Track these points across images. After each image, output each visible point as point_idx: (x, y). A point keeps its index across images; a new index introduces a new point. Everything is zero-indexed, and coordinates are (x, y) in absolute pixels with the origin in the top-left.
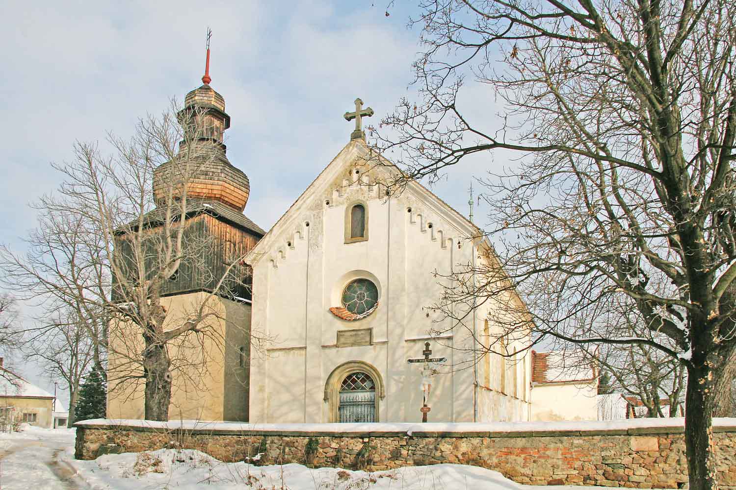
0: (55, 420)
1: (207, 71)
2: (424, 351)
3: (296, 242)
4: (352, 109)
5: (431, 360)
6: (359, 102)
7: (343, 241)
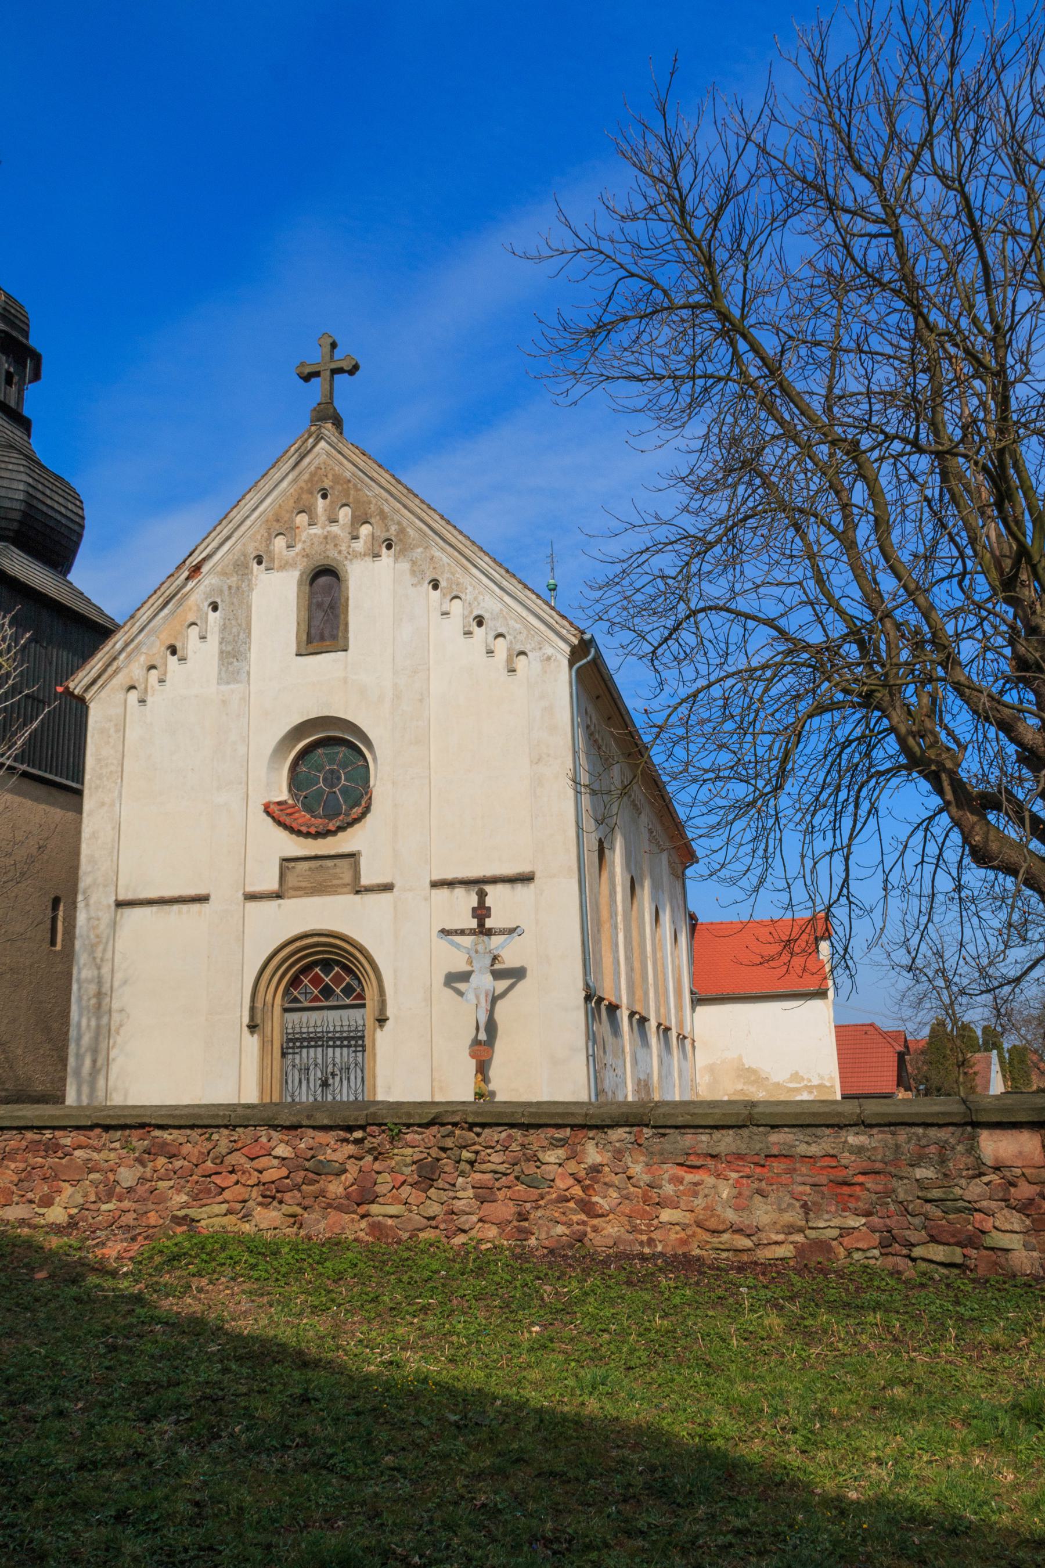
4: (316, 357)
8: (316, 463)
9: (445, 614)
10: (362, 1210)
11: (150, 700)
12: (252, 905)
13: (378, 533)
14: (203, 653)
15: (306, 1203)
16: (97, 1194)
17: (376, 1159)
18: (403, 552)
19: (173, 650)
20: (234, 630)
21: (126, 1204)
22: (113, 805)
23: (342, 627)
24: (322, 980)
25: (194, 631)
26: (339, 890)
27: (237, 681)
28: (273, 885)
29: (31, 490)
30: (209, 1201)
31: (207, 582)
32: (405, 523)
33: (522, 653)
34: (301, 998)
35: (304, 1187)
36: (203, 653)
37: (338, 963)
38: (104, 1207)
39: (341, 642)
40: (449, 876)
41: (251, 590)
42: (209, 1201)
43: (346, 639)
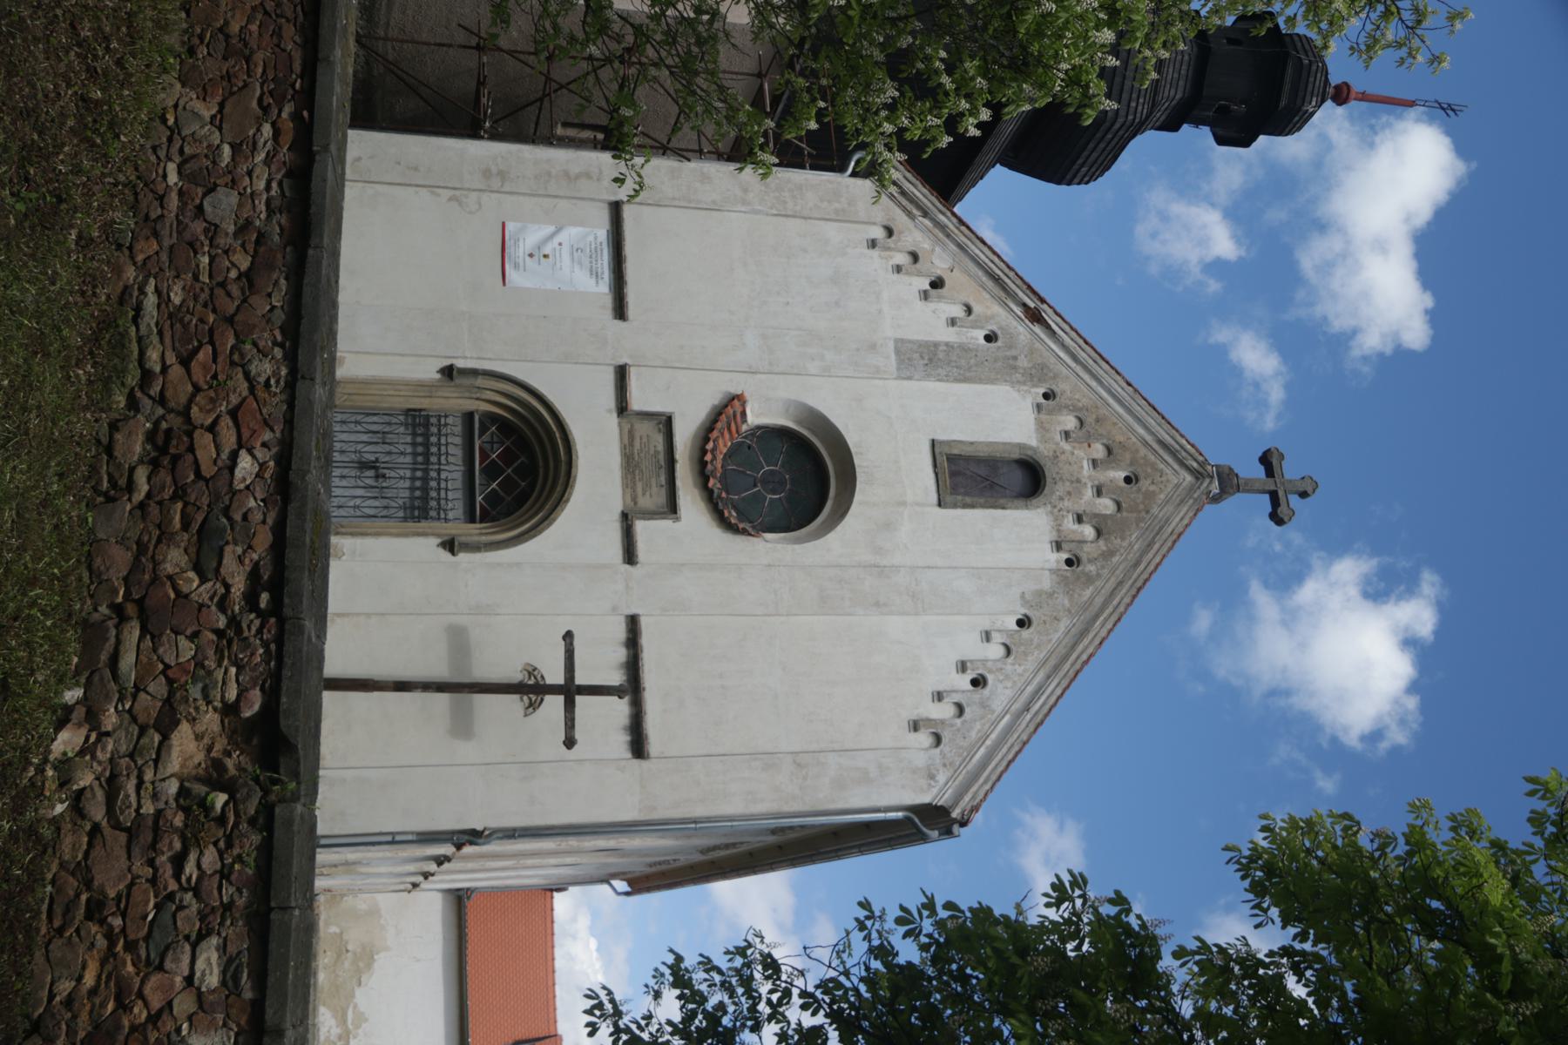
4: (1291, 470)
7: (941, 437)
8: (1168, 471)
9: (987, 637)
10: (131, 609)
11: (875, 253)
12: (609, 378)
13: (1087, 548)
14: (931, 322)
15: (154, 510)
16: (194, 156)
17: (220, 633)
18: (1064, 581)
19: (937, 284)
20: (963, 362)
21: (173, 201)
22: (744, 202)
23: (968, 500)
24: (511, 466)
25: (958, 311)
26: (629, 491)
27: (900, 362)
28: (637, 402)
29: (1107, 124)
30: (168, 340)
31: (1021, 329)
32: (1099, 583)
33: (938, 740)
34: (486, 437)
35: (180, 505)
36: (931, 322)
37: (532, 486)
38: (172, 168)
39: (949, 499)
40: (645, 641)
41: (1013, 384)
42: (168, 340)
43: (955, 506)
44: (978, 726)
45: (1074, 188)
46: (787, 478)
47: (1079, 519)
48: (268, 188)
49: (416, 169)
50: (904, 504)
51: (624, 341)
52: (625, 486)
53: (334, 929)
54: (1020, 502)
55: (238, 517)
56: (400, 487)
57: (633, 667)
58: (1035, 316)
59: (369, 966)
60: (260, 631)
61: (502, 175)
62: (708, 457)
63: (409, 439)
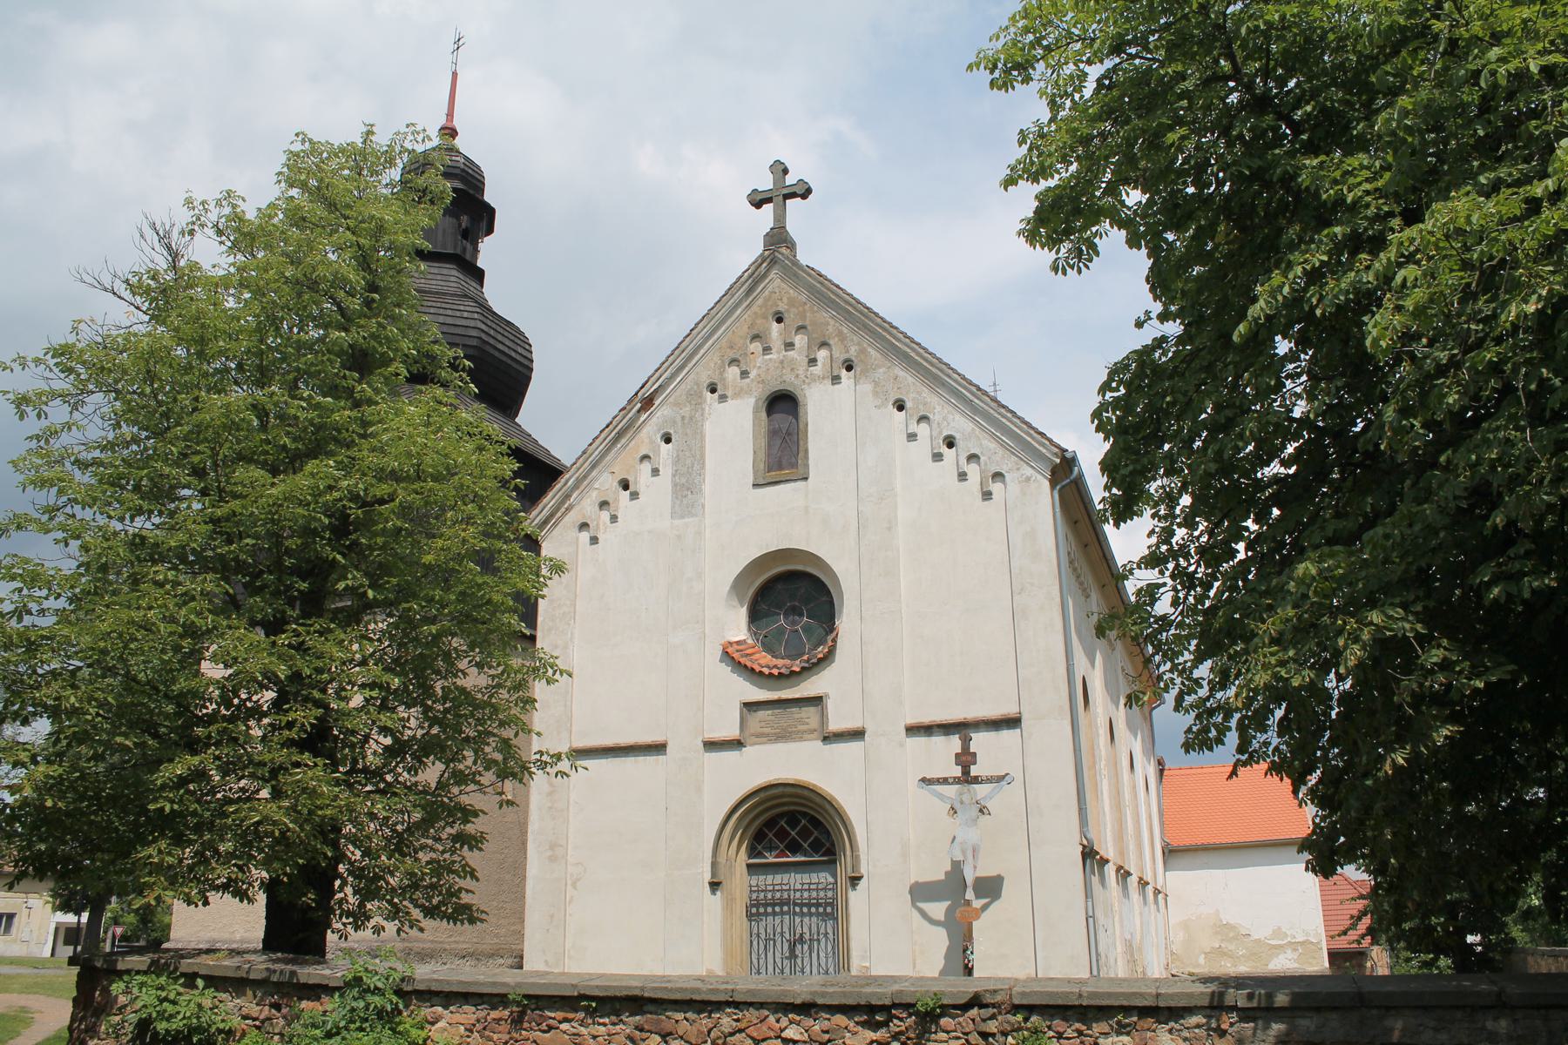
0: (57, 929)
1: (450, 115)
2: (992, 84)
3: (642, 478)
4: (766, 183)
5: (976, 780)
6: (780, 169)
7: (751, 480)
9: (912, 437)
20: (688, 462)
25: (646, 467)
29: (484, 336)
36: (655, 490)
37: (805, 814)
39: (801, 470)
43: (807, 466)
44: (985, 442)
45: (534, 357)
46: (792, 600)
47: (813, 361)
48: (604, 1025)
49: (552, 916)
50: (806, 508)
51: (684, 744)
52: (801, 739)
53: (1202, 960)
54: (801, 411)
55: (827, 1036)
56: (807, 925)
57: (947, 728)
58: (648, 403)
59: (1229, 926)
60: (901, 1019)
61: (552, 847)
62: (775, 672)
63: (770, 918)
